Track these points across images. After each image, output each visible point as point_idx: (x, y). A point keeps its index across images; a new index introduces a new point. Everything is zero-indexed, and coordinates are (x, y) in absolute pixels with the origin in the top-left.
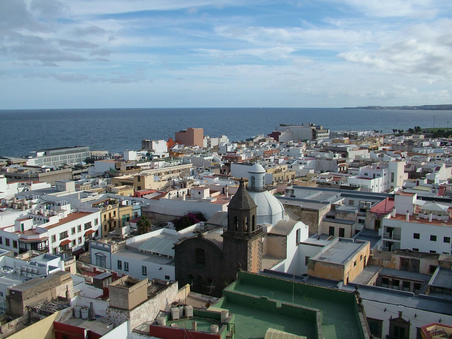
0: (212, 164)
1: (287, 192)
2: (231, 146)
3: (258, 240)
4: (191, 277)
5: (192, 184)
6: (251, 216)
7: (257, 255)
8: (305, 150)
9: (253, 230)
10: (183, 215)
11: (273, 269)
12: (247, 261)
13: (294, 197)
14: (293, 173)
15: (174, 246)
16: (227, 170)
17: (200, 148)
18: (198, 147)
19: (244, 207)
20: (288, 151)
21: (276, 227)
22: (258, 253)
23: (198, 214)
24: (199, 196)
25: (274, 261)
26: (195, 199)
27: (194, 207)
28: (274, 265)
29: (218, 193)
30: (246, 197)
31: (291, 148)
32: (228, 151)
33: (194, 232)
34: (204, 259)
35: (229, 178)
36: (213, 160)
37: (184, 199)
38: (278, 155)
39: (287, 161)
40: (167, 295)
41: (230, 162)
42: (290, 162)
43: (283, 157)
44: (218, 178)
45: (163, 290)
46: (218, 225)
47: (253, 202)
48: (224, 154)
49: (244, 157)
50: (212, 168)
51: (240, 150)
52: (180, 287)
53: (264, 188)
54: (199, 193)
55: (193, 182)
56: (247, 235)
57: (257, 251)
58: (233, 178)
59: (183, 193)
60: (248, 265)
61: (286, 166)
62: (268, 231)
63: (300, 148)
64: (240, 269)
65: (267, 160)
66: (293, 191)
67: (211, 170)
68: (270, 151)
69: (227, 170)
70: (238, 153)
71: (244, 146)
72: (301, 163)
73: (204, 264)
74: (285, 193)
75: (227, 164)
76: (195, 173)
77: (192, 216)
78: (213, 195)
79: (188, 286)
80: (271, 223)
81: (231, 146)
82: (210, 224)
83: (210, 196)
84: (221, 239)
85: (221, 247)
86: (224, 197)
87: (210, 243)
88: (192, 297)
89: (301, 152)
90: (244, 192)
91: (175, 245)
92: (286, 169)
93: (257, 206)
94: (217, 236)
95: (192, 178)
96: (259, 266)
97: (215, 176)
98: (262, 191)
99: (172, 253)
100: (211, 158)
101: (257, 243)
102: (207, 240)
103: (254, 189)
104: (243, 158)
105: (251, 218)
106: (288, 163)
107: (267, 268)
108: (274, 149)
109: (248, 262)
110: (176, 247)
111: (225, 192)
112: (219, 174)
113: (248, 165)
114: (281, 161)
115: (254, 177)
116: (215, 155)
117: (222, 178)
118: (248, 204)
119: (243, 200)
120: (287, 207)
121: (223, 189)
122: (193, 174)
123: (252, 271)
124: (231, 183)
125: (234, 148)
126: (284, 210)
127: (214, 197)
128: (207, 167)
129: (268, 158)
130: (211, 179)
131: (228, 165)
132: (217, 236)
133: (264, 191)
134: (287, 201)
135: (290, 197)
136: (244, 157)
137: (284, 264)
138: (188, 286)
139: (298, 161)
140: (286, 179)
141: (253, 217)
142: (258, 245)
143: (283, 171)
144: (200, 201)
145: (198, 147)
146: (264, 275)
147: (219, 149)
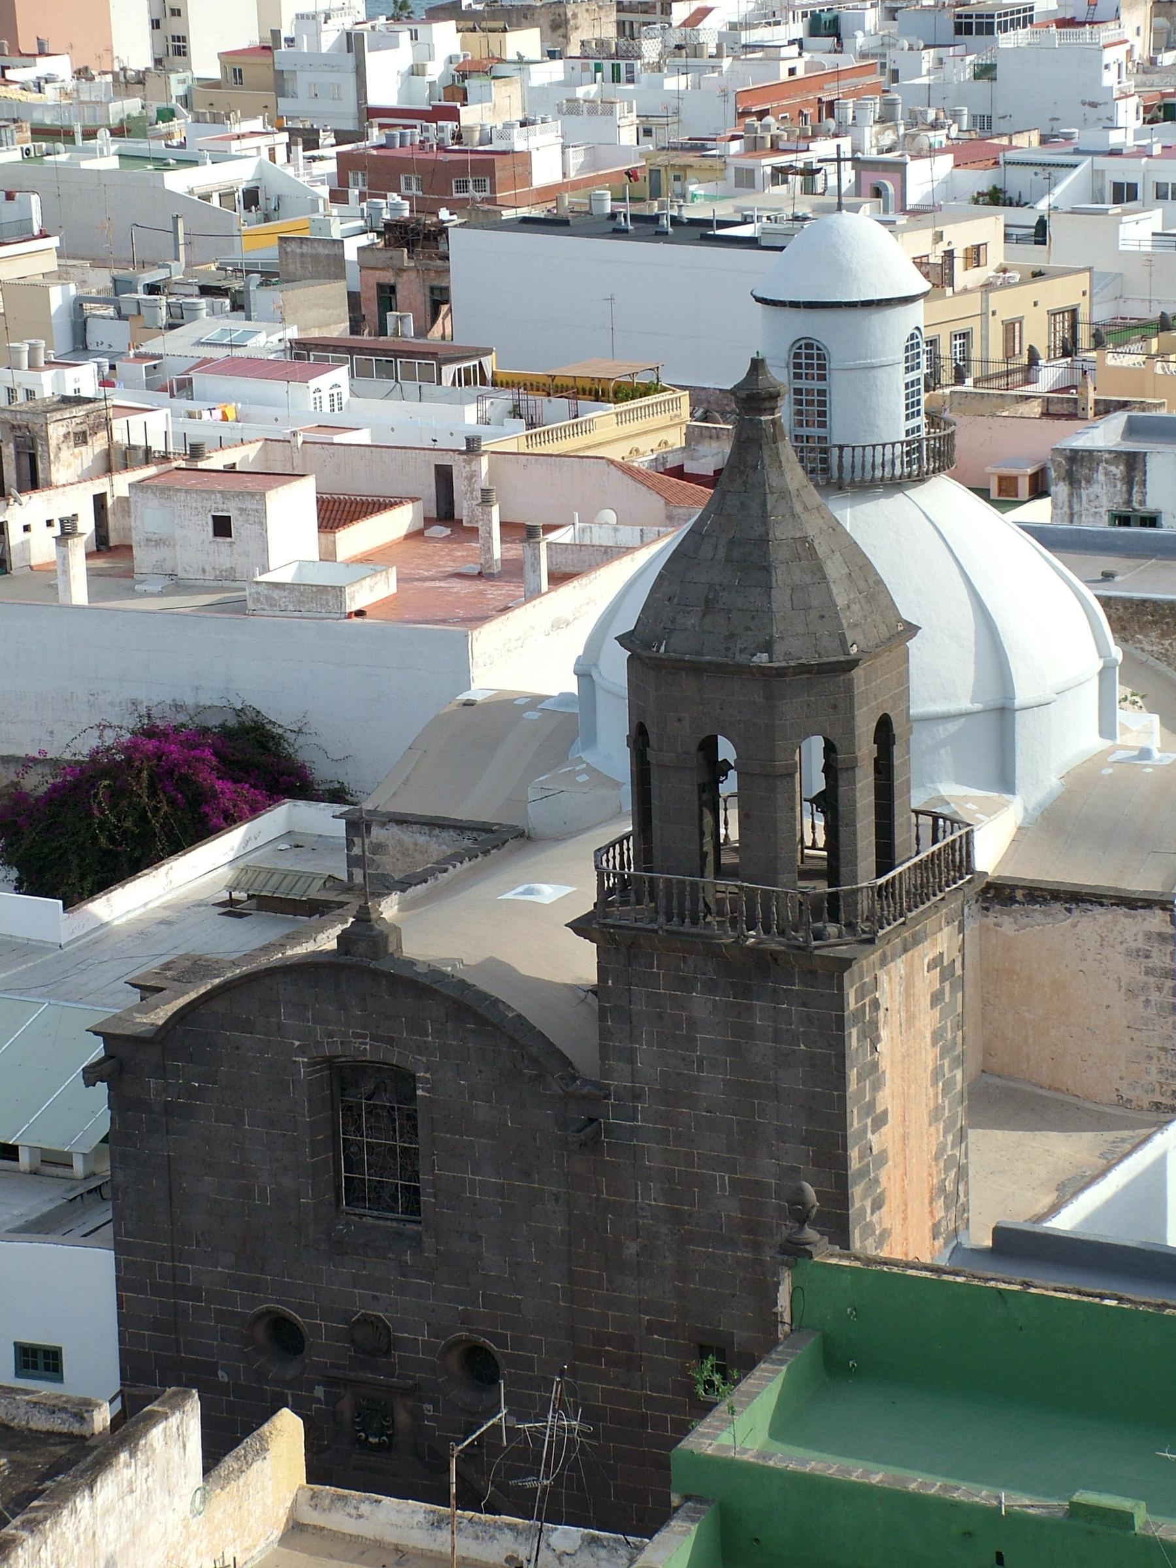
0: (257, 243)
1: (1072, 480)
2: (403, 54)
3: (927, 951)
4: (285, 1335)
5: (99, 443)
6: (865, 729)
7: (925, 1096)
8: (1142, 47)
9: (885, 859)
10: (85, 746)
11: (1065, 1222)
12: (844, 1162)
13: (1151, 521)
14: (1065, 292)
15: (97, 1050)
16: (411, 289)
17: (82, 73)
18: (60, 67)
19: (792, 647)
20: (986, 72)
21: (1053, 823)
22: (937, 1073)
23: (226, 733)
24: (222, 553)
25: (1065, 1148)
26: (177, 584)
27: (188, 669)
28: (1071, 1187)
29: (395, 523)
30: (806, 543)
31: (1008, 40)
32: (375, 99)
33: (231, 909)
34: (410, 1155)
35: (449, 371)
36: (251, 197)
37: (79, 593)
38: (886, 118)
39: (980, 179)
40: (110, 1537)
41: (424, 207)
42: (1017, 181)
43: (938, 138)
44: (341, 375)
45: (65, 1495)
46: (485, 828)
47: (873, 589)
48: (342, 137)
49: (549, 160)
50: (269, 277)
51: (498, 90)
52: (222, 1442)
53: (913, 448)
54: (222, 527)
55: (107, 424)
56: (832, 907)
57: (929, 1056)
58: (490, 364)
59: (68, 529)
60: (856, 1190)
61: (988, 228)
62: (989, 856)
63: (1106, 33)
64: (810, 1233)
65: (780, 174)
66: (1133, 464)
67: (260, 298)
68: (795, 85)
69: (411, 289)
70: (469, 115)
71: (524, 42)
72: (1125, 193)
73: (413, 1207)
74: (1060, 490)
75: (399, 235)
76: (105, 329)
77: (175, 752)
78: (357, 538)
79: (287, 1432)
80: (1005, 781)
81: (403, 54)
82: (401, 820)
83: (328, 555)
84: (581, 962)
85: (575, 1037)
86: (463, 556)
87: (463, 1007)
88: (337, 1537)
89: (1109, 79)
90: (784, 494)
91: (108, 1038)
92: (996, 254)
93: (912, 630)
94: (527, 928)
95: (83, 378)
96: (952, 1200)
97: (307, 353)
98: (896, 484)
99: (80, 1119)
100: (238, 174)
101: (928, 981)
102: (437, 975)
103: (842, 473)
104: (546, 171)
105: (866, 749)
106: (996, 197)
107: (1017, 1217)
108: (829, 61)
109: (854, 1164)
110: (123, 1063)
111: (464, 508)
112: (339, 329)
113: (619, 233)
114: (924, 178)
115: (817, 337)
116: (248, 154)
117: (386, 371)
118: (829, 612)
119: (780, 576)
120: (1128, 617)
121: (444, 476)
122: (81, 345)
123: (894, 1250)
124: (471, 414)
125: (436, 70)
126: (1117, 653)
127: (370, 561)
128: (210, 271)
129: (799, 160)
130: (277, 388)
131: (414, 238)
132: (527, 928)
133: (920, 479)
134: (1108, 562)
135: (1102, 525)
136: (549, 160)
137: (1160, 1165)
138: (287, 1432)
139: (1097, 174)
140: (996, 351)
141: (885, 732)
142: (936, 998)
143: (964, 277)
144: (238, 607)
145: (60, 67)
146: (1006, 1280)
147: (280, 84)
